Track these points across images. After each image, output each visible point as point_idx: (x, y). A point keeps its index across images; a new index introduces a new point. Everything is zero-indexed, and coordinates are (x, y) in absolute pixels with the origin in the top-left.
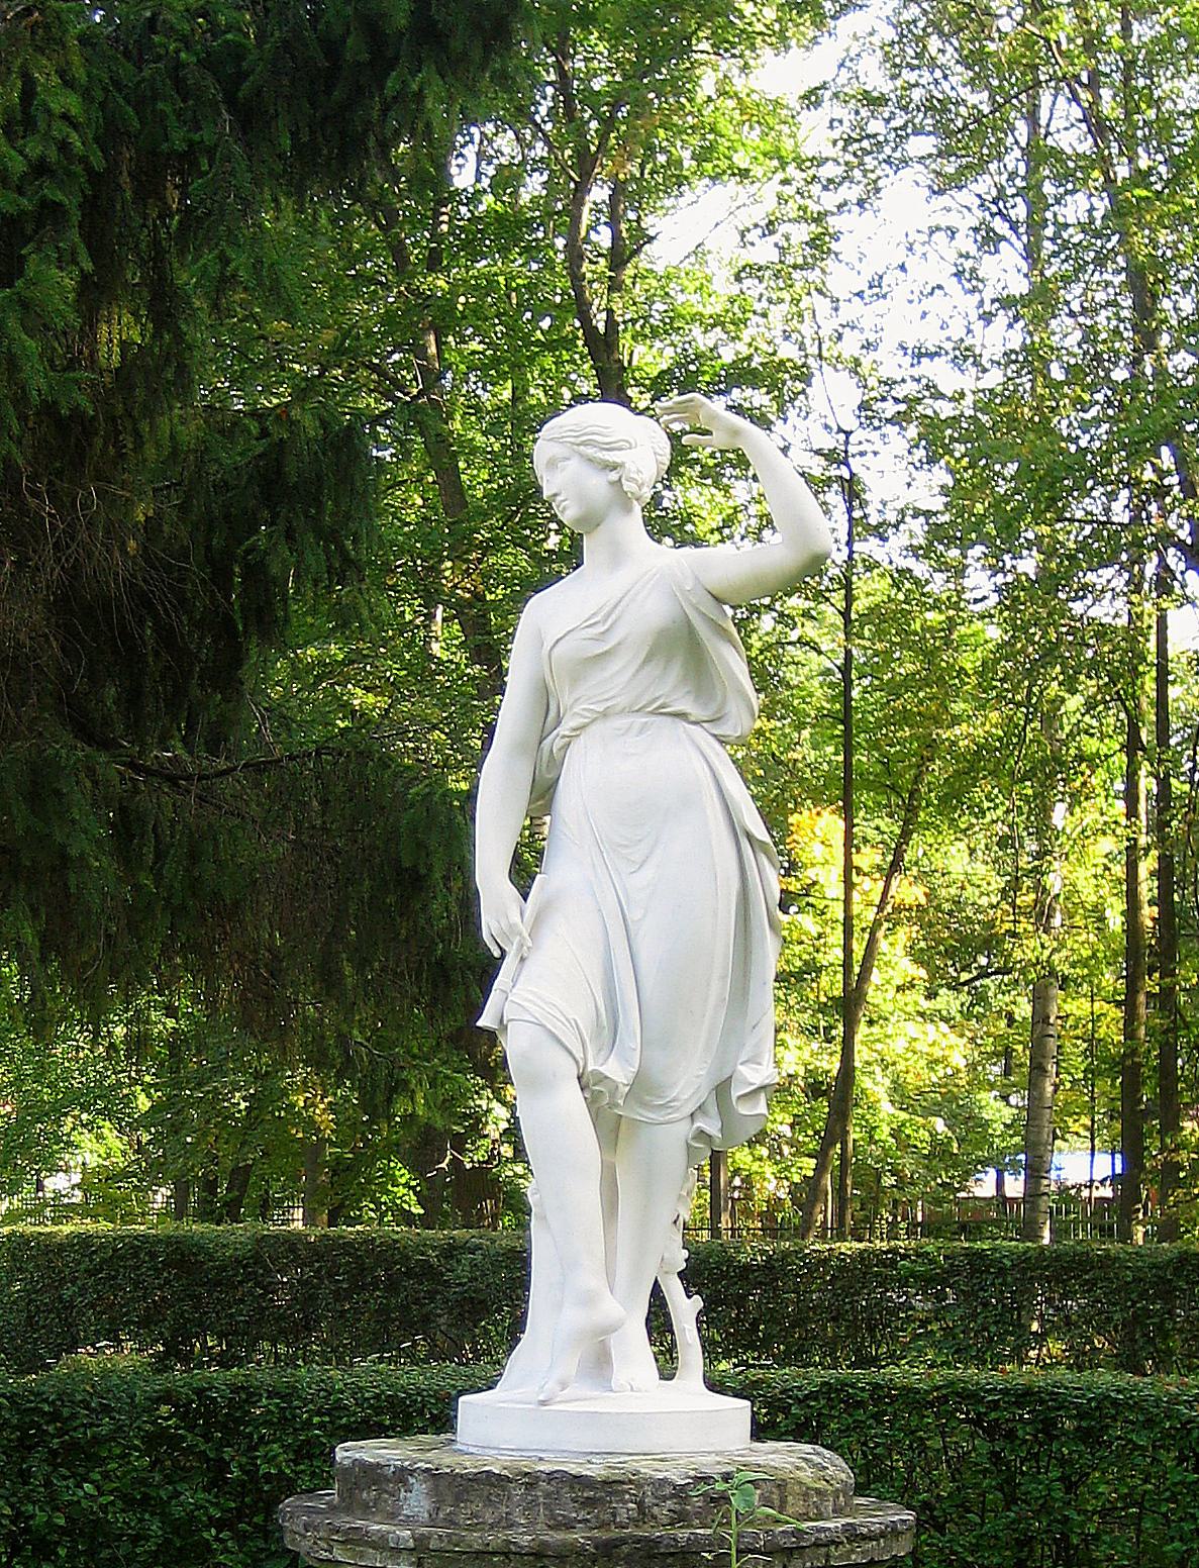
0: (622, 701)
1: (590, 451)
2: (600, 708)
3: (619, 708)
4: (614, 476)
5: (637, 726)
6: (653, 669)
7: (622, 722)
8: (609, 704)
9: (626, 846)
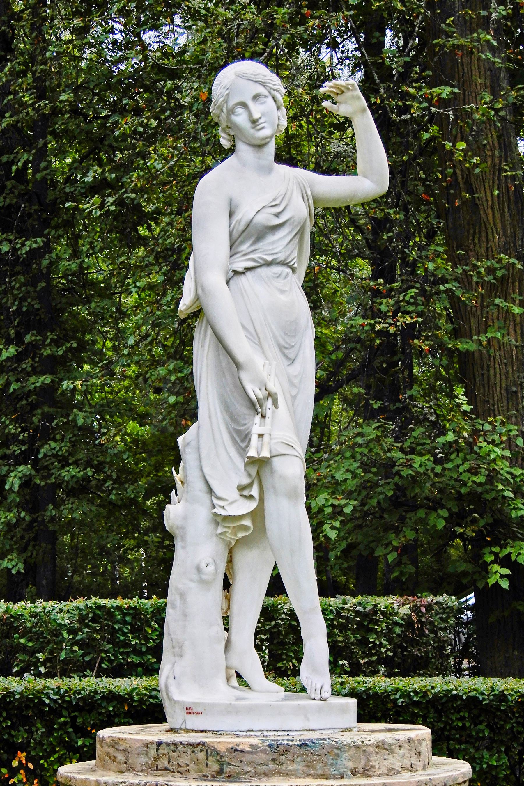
0: (281, 257)
2: (269, 258)
8: (274, 257)
9: (287, 348)
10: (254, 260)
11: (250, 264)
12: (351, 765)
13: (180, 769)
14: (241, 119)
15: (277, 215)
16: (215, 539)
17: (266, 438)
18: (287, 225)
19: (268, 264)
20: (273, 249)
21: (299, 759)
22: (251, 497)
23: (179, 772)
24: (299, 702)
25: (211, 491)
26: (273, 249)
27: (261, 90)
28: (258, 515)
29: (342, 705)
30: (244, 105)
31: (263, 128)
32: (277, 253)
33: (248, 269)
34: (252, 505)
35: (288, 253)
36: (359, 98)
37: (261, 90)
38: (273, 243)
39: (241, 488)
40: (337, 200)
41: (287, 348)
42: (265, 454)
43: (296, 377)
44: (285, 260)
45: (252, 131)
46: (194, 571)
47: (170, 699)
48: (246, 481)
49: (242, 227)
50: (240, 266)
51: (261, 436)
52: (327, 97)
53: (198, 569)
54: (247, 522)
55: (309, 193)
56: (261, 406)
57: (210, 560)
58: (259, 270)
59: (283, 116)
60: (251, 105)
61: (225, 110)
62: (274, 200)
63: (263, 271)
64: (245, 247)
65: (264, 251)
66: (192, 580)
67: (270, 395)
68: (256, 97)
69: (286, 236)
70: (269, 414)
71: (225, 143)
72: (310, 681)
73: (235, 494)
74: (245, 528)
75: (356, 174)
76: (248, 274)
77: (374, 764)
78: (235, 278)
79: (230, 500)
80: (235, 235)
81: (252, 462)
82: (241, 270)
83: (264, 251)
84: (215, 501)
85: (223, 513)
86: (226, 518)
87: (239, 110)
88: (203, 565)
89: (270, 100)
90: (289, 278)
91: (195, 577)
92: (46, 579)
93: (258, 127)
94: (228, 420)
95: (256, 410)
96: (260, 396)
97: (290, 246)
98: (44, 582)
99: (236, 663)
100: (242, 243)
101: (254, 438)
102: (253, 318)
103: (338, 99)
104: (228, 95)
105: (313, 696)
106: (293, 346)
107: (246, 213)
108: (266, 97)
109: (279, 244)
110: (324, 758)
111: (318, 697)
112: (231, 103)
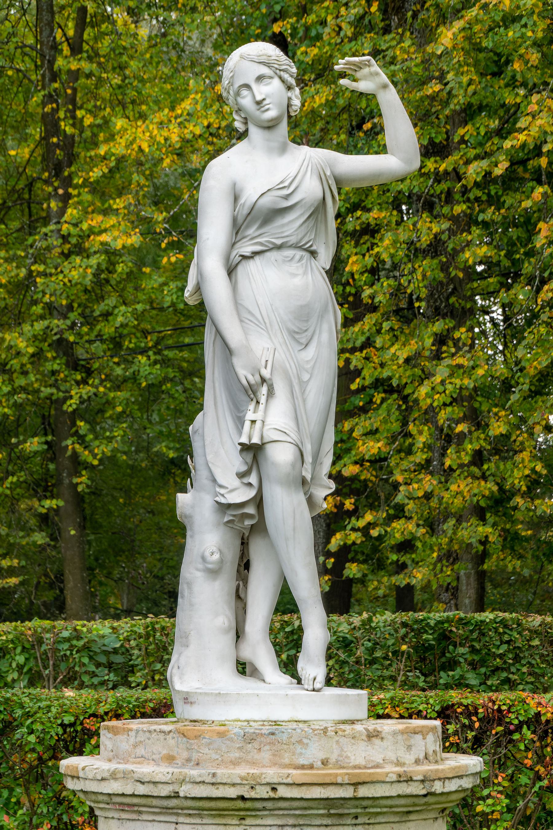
0: (293, 240)
2: (279, 242)
3: (291, 243)
5: (297, 257)
7: (289, 253)
9: (297, 333)
10: (261, 244)
11: (258, 248)
12: (322, 755)
13: (154, 757)
14: (246, 101)
15: (287, 197)
16: (222, 528)
17: (258, 424)
18: (299, 206)
19: (279, 247)
20: (282, 232)
21: (267, 747)
22: (250, 485)
23: (153, 760)
24: (296, 691)
25: (214, 481)
26: (282, 232)
27: (265, 70)
28: (258, 501)
29: (339, 696)
30: (247, 86)
31: (268, 110)
32: (287, 236)
33: (256, 253)
34: (251, 493)
35: (300, 237)
36: (377, 74)
37: (265, 70)
38: (283, 226)
39: (241, 475)
40: (362, 178)
41: (297, 333)
42: (256, 440)
43: (308, 362)
44: (297, 243)
45: (258, 113)
46: (200, 560)
47: (174, 689)
48: (244, 468)
49: (245, 211)
50: (247, 249)
51: (253, 422)
52: (343, 75)
53: (203, 559)
54: (250, 510)
55: (328, 173)
56: (254, 393)
57: (215, 549)
58: (268, 254)
59: (296, 97)
60: (254, 86)
61: (231, 92)
62: (282, 182)
63: (273, 255)
64: (251, 231)
65: (272, 234)
66: (198, 570)
67: (263, 380)
68: (260, 79)
69: (297, 218)
70: (263, 400)
71: (238, 125)
72: (304, 672)
73: (236, 482)
74: (250, 516)
75: (386, 153)
76: (257, 258)
77: (349, 755)
78: (244, 262)
79: (230, 488)
80: (240, 219)
81: (246, 448)
82: (248, 254)
83: (272, 234)
84: (218, 489)
85: (223, 501)
86: (230, 506)
87: (245, 92)
88: (207, 554)
89: (276, 82)
90: (304, 261)
91: (200, 566)
92: (470, 597)
93: (263, 109)
94: (232, 406)
95: (249, 396)
96: (252, 381)
97: (303, 228)
98: (467, 601)
99: (246, 654)
100: (248, 227)
101: (247, 424)
102: (259, 303)
103: (358, 75)
104: (232, 77)
105: (306, 687)
106: (306, 331)
107: (250, 195)
108: (271, 78)
109: (290, 226)
110: (291, 747)
111: (311, 688)
112: (236, 86)
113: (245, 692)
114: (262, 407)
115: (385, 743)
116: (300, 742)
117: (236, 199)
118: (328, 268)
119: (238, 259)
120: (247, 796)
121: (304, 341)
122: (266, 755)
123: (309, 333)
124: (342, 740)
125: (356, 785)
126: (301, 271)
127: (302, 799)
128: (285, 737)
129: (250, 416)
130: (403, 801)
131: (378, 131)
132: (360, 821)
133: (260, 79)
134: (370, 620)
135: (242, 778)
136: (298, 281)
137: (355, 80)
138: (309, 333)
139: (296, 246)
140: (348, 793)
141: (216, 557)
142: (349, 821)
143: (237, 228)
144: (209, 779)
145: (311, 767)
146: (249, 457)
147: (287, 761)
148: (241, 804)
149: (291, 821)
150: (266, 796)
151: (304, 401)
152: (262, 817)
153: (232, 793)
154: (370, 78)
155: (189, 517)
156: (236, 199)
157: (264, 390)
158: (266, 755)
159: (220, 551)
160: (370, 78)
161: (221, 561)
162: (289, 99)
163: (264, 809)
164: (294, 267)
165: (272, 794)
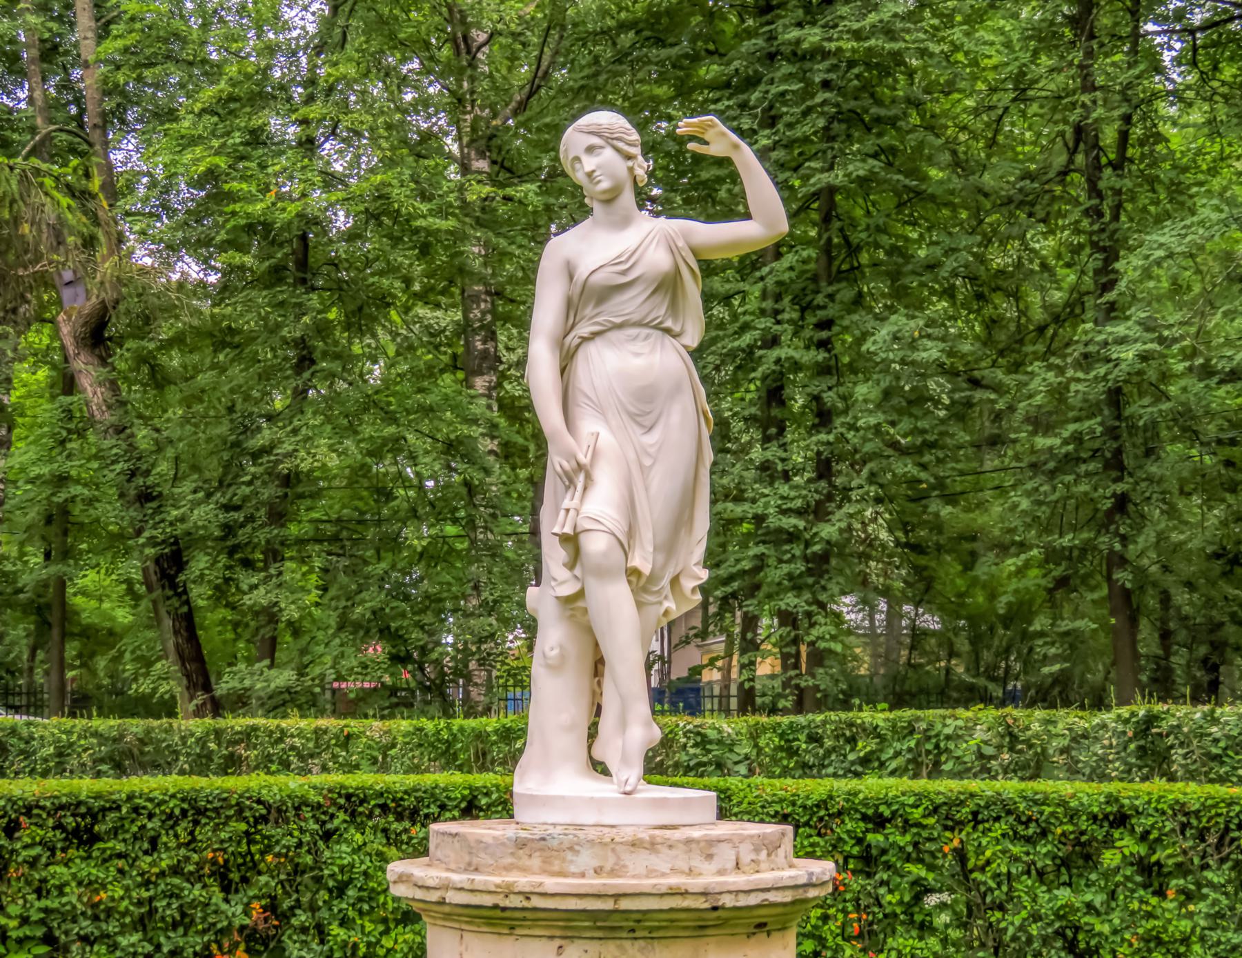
0: (635, 317)
1: (620, 145)
2: (618, 320)
4: (630, 163)
6: (657, 298)
7: (633, 331)
15: (624, 273)
17: (572, 513)
33: (595, 335)
37: (596, 141)
50: (584, 329)
51: (568, 510)
55: (681, 244)
63: (614, 335)
64: (589, 311)
67: (580, 467)
76: (598, 341)
100: (585, 306)
107: (582, 272)
109: (629, 304)
113: (589, 795)
114: (578, 494)
115: (673, 852)
116: (571, 848)
117: (571, 277)
118: (695, 345)
119: (577, 341)
120: (502, 905)
121: (648, 423)
122: (536, 862)
123: (652, 417)
124: (619, 848)
125: (617, 897)
126: (646, 350)
127: (556, 910)
128: (555, 843)
129: (567, 503)
130: (683, 915)
131: (740, 196)
132: (637, 934)
133: (590, 149)
134: (1213, 711)
135: (498, 886)
136: (657, 358)
137: (707, 143)
138: (652, 417)
139: (639, 324)
140: (608, 905)
141: (556, 652)
142: (624, 935)
143: (572, 308)
144: (467, 886)
145: (583, 875)
146: (570, 547)
147: (556, 868)
148: (499, 913)
149: (558, 933)
150: (519, 905)
151: (647, 489)
152: (529, 927)
153: (488, 900)
154: (717, 137)
155: (536, 610)
156: (571, 277)
157: (581, 477)
158: (536, 862)
159: (561, 647)
160: (717, 137)
161: (562, 657)
162: (631, 170)
163: (525, 919)
164: (637, 347)
165: (526, 904)
